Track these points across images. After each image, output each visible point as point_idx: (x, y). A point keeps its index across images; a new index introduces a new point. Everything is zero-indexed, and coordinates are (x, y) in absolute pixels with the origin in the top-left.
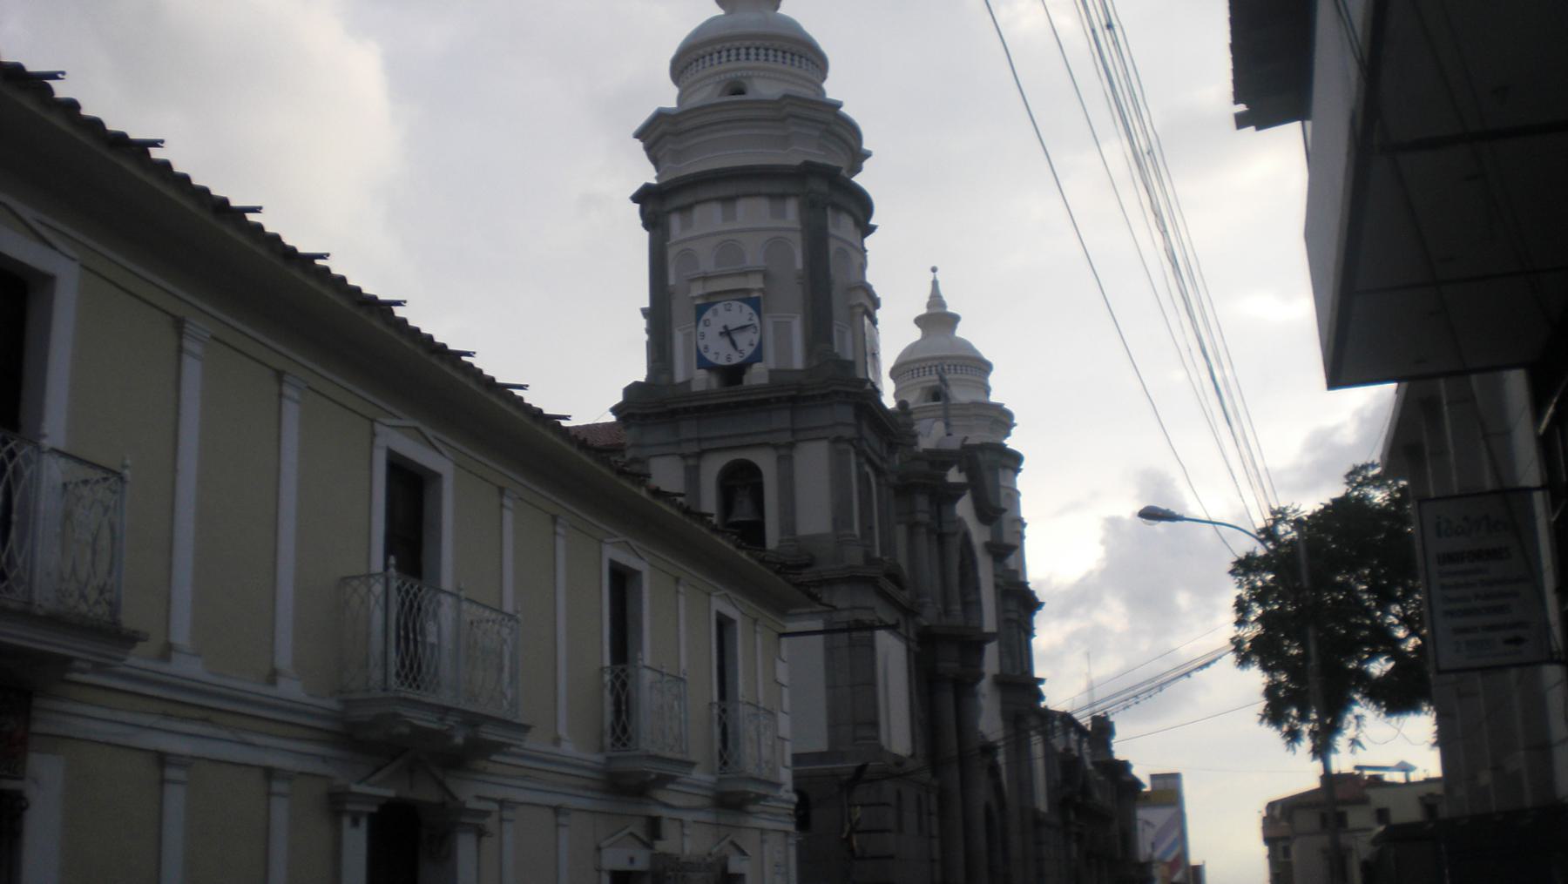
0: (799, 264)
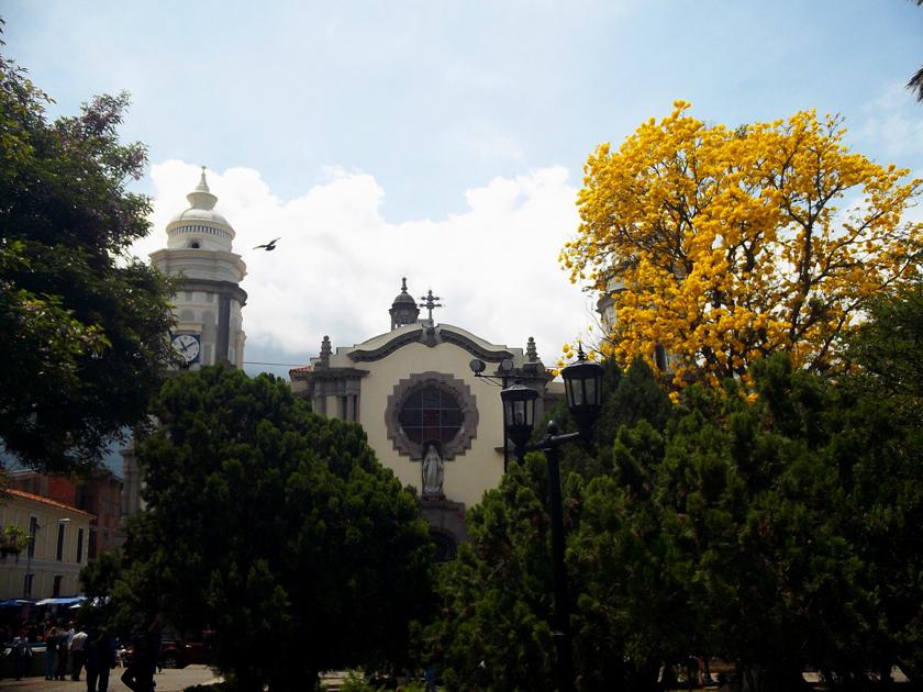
0: (217, 322)
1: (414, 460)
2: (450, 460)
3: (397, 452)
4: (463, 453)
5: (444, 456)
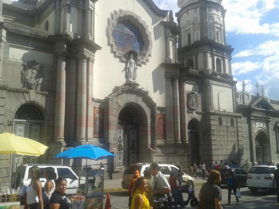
1: (122, 61)
2: (140, 65)
3: (113, 55)
4: (144, 63)
5: (138, 63)
